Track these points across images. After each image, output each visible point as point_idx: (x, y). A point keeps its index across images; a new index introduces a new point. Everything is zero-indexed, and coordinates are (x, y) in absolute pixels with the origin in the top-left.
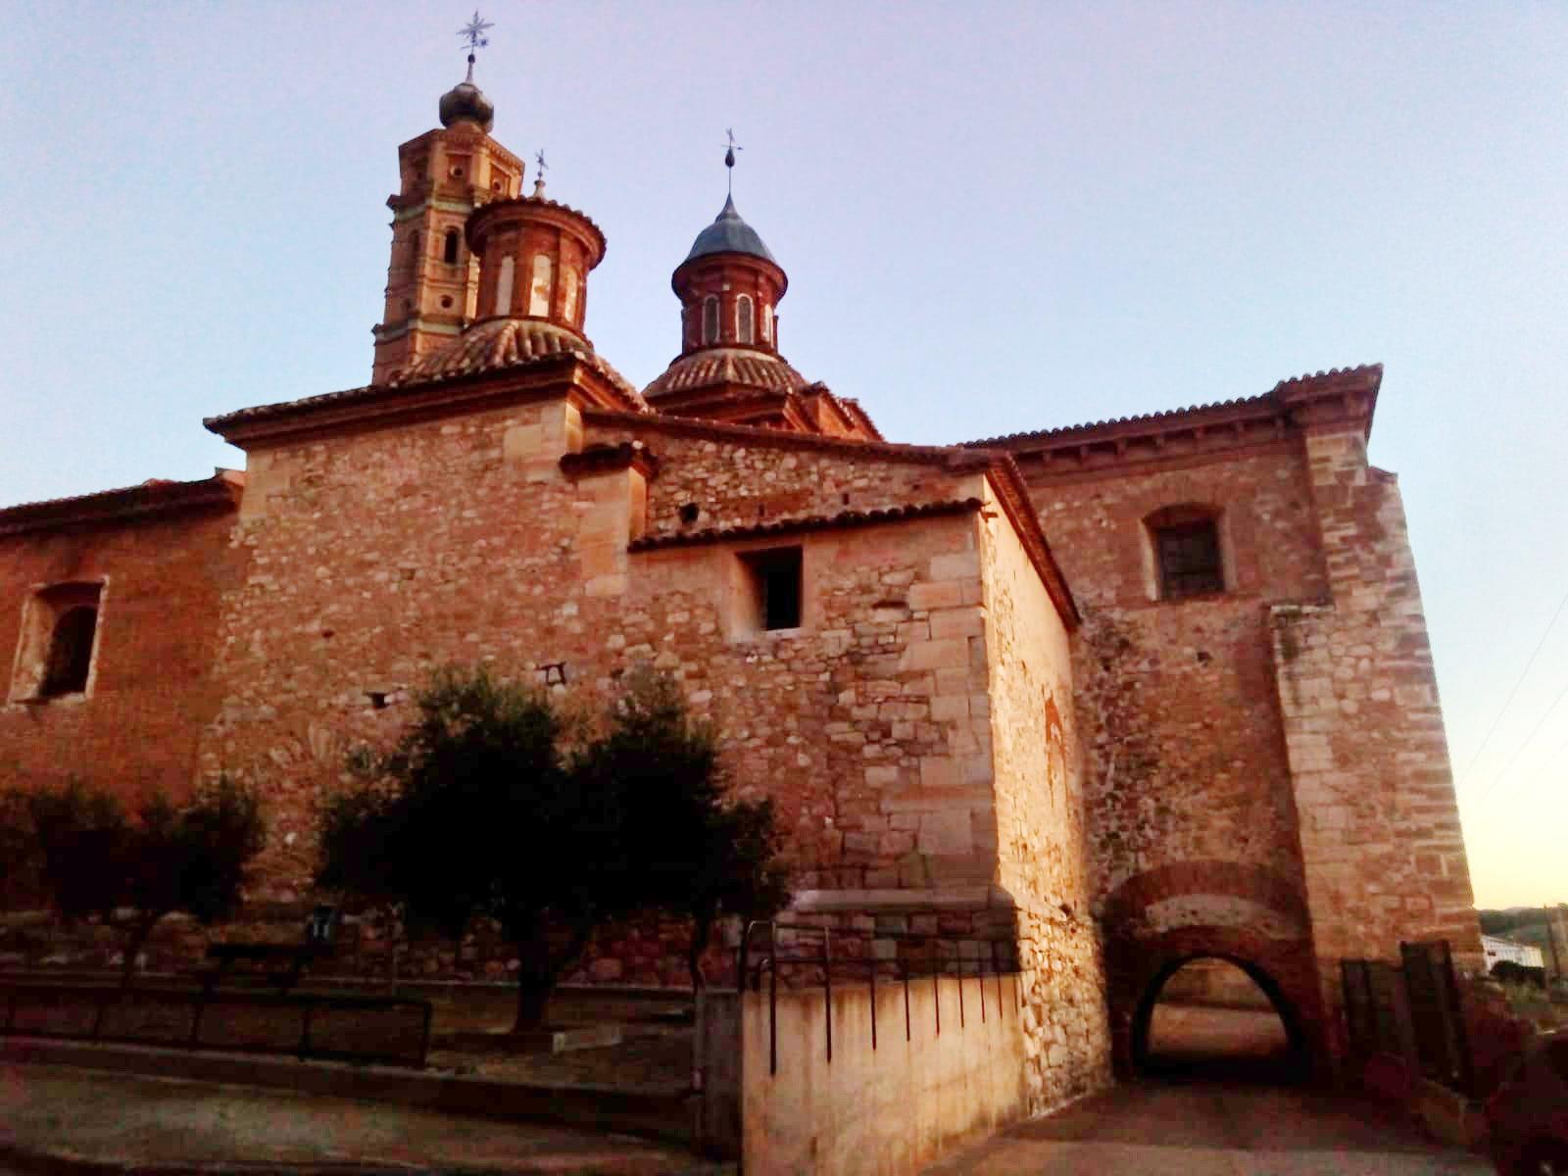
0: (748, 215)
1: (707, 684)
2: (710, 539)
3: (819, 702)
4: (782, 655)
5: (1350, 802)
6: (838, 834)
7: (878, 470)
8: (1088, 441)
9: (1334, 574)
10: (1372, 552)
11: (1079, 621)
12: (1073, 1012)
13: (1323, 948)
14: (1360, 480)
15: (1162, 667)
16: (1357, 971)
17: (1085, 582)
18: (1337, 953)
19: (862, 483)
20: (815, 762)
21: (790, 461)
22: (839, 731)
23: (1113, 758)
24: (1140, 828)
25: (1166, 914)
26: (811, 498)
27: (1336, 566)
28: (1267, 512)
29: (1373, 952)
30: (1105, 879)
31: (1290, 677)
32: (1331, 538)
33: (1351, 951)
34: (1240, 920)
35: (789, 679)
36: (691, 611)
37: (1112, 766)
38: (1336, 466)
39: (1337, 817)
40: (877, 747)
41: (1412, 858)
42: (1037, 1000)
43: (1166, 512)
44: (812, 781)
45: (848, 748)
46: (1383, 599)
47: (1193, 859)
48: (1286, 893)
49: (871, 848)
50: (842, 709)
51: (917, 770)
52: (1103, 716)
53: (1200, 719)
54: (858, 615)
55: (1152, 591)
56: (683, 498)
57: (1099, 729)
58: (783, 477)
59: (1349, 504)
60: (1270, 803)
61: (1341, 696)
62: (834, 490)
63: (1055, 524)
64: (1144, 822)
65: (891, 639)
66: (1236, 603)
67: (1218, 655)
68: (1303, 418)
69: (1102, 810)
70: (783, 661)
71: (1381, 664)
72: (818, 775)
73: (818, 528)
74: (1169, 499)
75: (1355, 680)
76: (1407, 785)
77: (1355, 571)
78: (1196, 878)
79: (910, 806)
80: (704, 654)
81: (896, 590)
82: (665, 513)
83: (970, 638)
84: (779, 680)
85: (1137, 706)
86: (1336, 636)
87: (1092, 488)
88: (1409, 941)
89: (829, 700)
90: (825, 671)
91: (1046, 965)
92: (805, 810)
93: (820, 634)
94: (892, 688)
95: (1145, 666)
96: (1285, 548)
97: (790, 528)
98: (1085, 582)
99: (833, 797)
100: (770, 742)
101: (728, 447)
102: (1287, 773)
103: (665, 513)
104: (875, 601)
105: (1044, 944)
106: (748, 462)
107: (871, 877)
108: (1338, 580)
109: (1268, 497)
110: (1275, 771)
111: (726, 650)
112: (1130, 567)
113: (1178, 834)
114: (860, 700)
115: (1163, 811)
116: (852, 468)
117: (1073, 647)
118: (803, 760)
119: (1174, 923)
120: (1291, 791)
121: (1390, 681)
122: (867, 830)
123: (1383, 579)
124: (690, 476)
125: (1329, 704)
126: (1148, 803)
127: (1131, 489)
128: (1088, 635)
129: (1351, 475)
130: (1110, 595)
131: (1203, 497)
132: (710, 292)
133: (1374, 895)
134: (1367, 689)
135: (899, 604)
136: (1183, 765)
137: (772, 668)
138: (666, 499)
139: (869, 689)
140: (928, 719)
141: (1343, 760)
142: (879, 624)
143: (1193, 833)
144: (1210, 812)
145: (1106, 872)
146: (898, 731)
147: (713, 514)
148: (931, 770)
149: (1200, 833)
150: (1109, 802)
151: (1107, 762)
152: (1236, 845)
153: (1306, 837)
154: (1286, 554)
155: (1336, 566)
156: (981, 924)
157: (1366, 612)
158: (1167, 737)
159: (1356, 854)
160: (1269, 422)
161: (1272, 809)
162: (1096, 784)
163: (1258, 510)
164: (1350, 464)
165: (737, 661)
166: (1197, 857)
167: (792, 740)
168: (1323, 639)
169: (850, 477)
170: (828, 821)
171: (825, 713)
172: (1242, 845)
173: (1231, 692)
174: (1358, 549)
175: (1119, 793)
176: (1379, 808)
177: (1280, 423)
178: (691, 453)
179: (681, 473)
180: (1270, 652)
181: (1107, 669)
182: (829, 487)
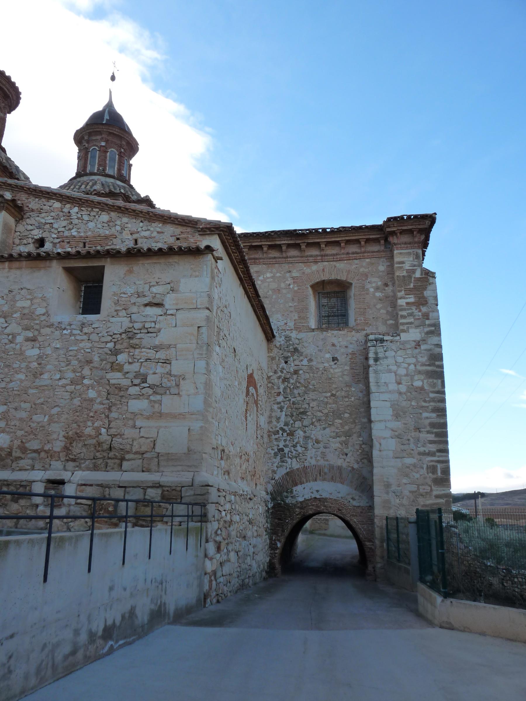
0: (119, 108)
1: (38, 345)
2: (48, 257)
3: (105, 360)
4: (85, 330)
5: (399, 437)
6: (109, 438)
7: (157, 226)
8: (286, 242)
9: (402, 321)
10: (420, 311)
11: (274, 336)
12: (244, 543)
13: (379, 511)
14: (418, 274)
15: (314, 363)
16: (394, 523)
17: (279, 316)
18: (385, 513)
19: (147, 234)
20: (99, 395)
21: (105, 217)
22: (115, 377)
23: (285, 409)
24: (294, 446)
25: (303, 493)
26: (114, 240)
27: (403, 317)
28: (372, 287)
29: (402, 513)
30: (274, 472)
31: (376, 372)
32: (401, 302)
33: (392, 513)
34: (340, 496)
35: (89, 345)
36: (31, 300)
37: (284, 413)
38: (407, 266)
39: (392, 444)
40: (137, 388)
41: (425, 466)
42: (218, 539)
43: (323, 283)
44: (96, 407)
45: (119, 388)
46: (423, 335)
47: (319, 463)
48: (365, 485)
49: (128, 447)
50: (118, 364)
51: (160, 402)
52: (282, 386)
53: (330, 391)
54: (134, 309)
55: (313, 323)
56: (37, 234)
57: (279, 394)
58: (99, 226)
59: (412, 286)
60: (360, 436)
61: (399, 383)
62: (130, 237)
63: (266, 284)
64: (297, 443)
65: (153, 325)
66: (353, 333)
67: (342, 359)
68: (393, 240)
69: (277, 436)
70: (86, 333)
71: (419, 368)
72: (101, 403)
73: (114, 255)
74: (326, 277)
75: (407, 375)
76: (425, 430)
77: (412, 320)
78: (320, 474)
79: (152, 423)
80: (37, 327)
81: (158, 296)
82: (25, 241)
83: (199, 327)
84: (82, 345)
85: (299, 383)
86: (400, 353)
87: (286, 267)
88: (420, 508)
89: (112, 359)
90: (111, 341)
91: (228, 518)
92: (89, 423)
93: (110, 318)
94: (151, 354)
95: (305, 362)
96: (379, 306)
97: (98, 255)
98: (279, 316)
99: (107, 417)
100: (73, 382)
101: (68, 206)
102: (370, 421)
103: (25, 241)
104: (146, 302)
105: (228, 506)
106: (79, 216)
107: (125, 464)
108: (403, 324)
109: (374, 280)
110: (365, 420)
111: (51, 326)
112: (303, 311)
113: (314, 450)
114: (130, 361)
115: (306, 438)
116: (141, 224)
117: (270, 350)
118: (92, 394)
119: (307, 497)
120: (371, 429)
121: (422, 377)
122: (125, 437)
123: (424, 325)
124: (43, 221)
125: (393, 387)
126: (300, 433)
127: (307, 270)
128: (278, 344)
129: (414, 271)
130: (291, 324)
131: (343, 277)
132: (95, 145)
133: (406, 484)
134: (412, 379)
135: (159, 305)
136: (319, 414)
137: (78, 337)
138: (27, 233)
139: (136, 353)
140: (169, 374)
141: (397, 416)
142: (147, 316)
143: (322, 449)
144: (331, 439)
145: (276, 469)
146: (151, 379)
147: (55, 245)
148: (168, 403)
149: (324, 450)
150: (281, 432)
151: (281, 411)
152: (341, 456)
153: (375, 453)
154: (379, 310)
155: (403, 317)
156: (187, 493)
157: (414, 341)
158: (313, 400)
159: (398, 463)
160: (376, 241)
161: (361, 439)
162: (275, 423)
163: (368, 286)
164: (415, 266)
165: (57, 333)
166: (322, 462)
167: (86, 382)
168: (393, 353)
169: (140, 229)
170: (103, 431)
171: (108, 366)
172: (345, 457)
173: (347, 378)
174: (414, 308)
175: (286, 428)
176: (412, 440)
177: (382, 242)
178: (45, 208)
179: (37, 219)
180: (367, 359)
181: (286, 362)
182: (126, 235)
